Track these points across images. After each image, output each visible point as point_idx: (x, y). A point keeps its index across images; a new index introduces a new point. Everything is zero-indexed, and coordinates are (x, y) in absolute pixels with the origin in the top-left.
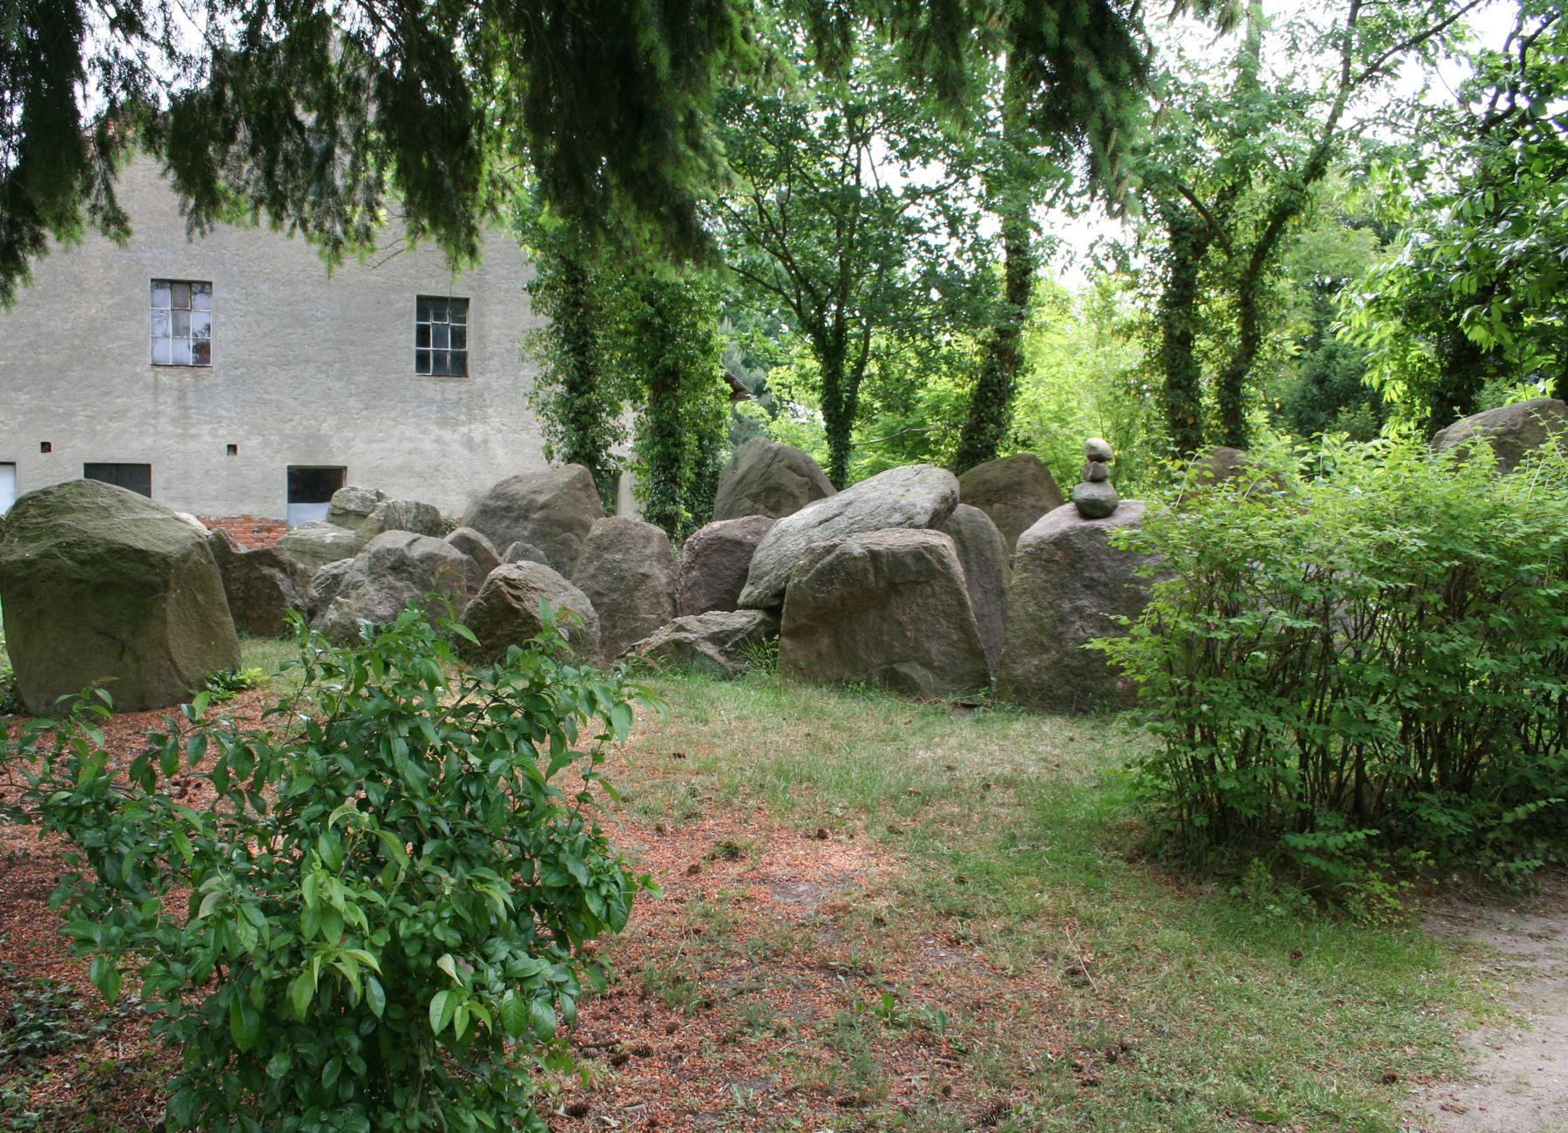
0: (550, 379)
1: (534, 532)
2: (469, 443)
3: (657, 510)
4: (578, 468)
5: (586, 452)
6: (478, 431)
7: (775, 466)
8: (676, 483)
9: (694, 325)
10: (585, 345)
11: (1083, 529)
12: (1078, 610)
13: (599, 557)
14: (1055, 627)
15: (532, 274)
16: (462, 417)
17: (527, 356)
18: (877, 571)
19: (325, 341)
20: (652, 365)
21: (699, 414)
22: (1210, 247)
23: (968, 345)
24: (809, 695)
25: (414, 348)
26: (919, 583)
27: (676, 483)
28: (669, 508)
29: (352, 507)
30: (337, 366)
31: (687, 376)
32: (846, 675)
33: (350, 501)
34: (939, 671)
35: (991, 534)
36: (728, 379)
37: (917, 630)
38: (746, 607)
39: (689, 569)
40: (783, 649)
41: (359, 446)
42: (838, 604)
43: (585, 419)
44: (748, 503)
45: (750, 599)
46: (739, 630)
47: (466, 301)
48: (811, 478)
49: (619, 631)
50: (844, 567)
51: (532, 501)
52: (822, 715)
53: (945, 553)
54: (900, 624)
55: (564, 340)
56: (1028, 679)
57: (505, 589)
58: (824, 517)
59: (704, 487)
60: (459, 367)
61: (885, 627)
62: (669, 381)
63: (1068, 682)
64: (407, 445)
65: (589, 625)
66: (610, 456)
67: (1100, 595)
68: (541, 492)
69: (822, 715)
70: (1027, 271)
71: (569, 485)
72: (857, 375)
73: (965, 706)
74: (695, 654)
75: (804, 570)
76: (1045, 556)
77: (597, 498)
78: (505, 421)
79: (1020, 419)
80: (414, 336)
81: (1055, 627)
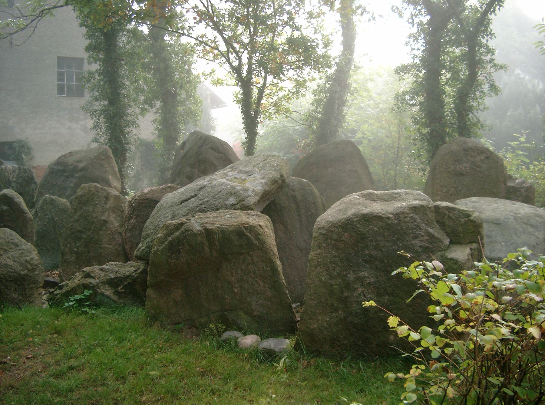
12: (361, 280)
16: (81, 117)
18: (211, 244)
44: (188, 169)
46: (128, 277)
54: (229, 282)
58: (184, 197)
76: (335, 237)
80: (56, 76)
81: (342, 292)
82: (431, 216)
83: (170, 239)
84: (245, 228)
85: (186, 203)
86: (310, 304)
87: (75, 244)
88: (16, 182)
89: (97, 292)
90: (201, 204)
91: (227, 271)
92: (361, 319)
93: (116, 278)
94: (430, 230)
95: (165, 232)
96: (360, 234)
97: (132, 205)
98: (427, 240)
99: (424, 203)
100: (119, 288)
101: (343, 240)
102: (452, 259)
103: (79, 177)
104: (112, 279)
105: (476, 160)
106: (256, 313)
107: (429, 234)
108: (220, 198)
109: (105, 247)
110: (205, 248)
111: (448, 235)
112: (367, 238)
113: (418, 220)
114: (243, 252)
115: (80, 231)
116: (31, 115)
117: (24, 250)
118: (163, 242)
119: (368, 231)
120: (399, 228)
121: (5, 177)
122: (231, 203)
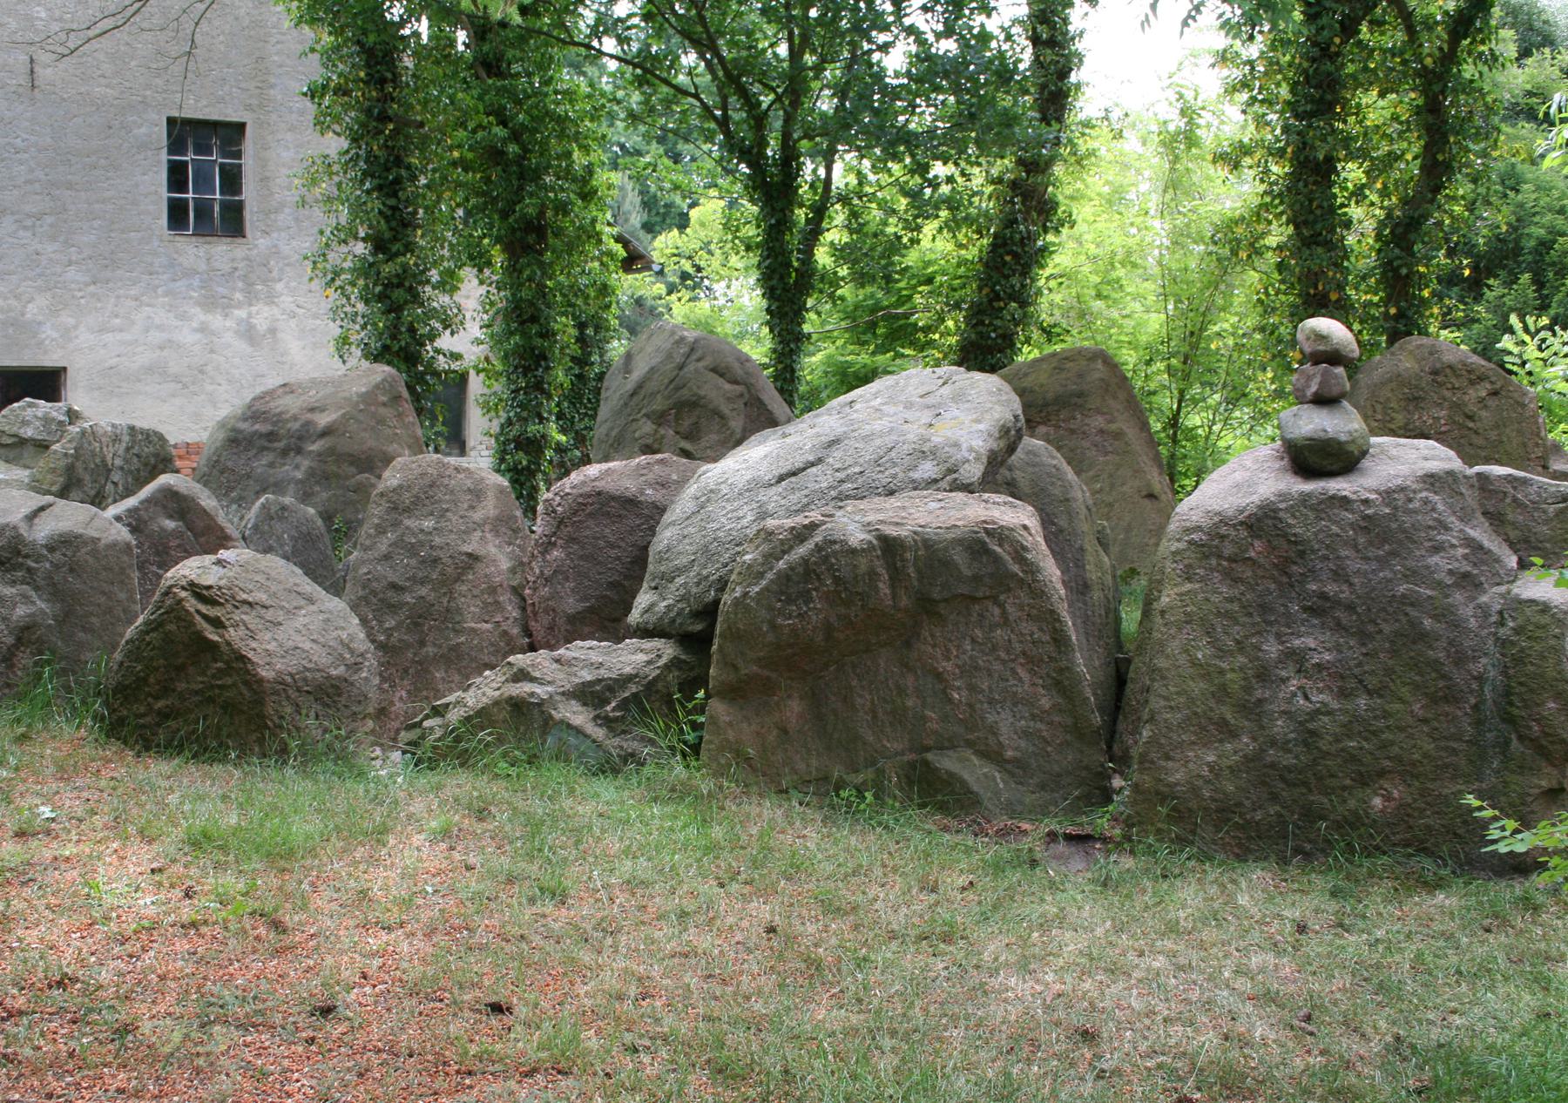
0: (346, 235)
1: (311, 473)
2: (249, 333)
3: (515, 431)
4: (383, 370)
5: (400, 339)
6: (262, 315)
7: (691, 367)
8: (543, 391)
9: (569, 154)
10: (398, 181)
11: (1304, 499)
12: (1296, 658)
13: (396, 524)
14: (1248, 689)
15: (314, 70)
16: (238, 296)
17: (309, 199)
18: (896, 575)
19: (27, 182)
20: (505, 215)
21: (578, 291)
22: (1364, 28)
23: (978, 179)
24: (763, 814)
25: (165, 194)
26: (974, 600)
27: (543, 391)
28: (533, 428)
29: (29, 432)
30: (49, 220)
31: (558, 233)
32: (836, 773)
33: (25, 423)
34: (1016, 768)
35: (1067, 487)
36: (619, 239)
37: (972, 688)
38: (645, 632)
39: (547, 546)
40: (713, 720)
41: (84, 337)
42: (819, 638)
43: (399, 294)
44: (647, 427)
45: (652, 619)
46: (630, 678)
47: (240, 128)
48: (749, 386)
49: (430, 650)
50: (831, 568)
51: (308, 423)
52: (796, 869)
53: (1028, 541)
54: (939, 676)
55: (365, 174)
56: (1195, 790)
57: (192, 604)
59: (588, 395)
60: (233, 223)
61: (910, 681)
62: (531, 239)
63: (1274, 798)
64: (156, 337)
65: (356, 667)
66: (438, 351)
67: (1339, 626)
68: (322, 410)
69: (796, 869)
70: (1064, 74)
71: (368, 398)
72: (814, 232)
73: (1070, 838)
74: (548, 724)
75: (752, 573)
76: (1228, 550)
77: (412, 417)
78: (301, 300)
79: (1051, 298)
80: (163, 176)
81: (1248, 689)
82: (1471, 497)
83: (781, 564)
84: (987, 531)
85: (793, 479)
86: (1166, 721)
87: (381, 622)
88: (122, 468)
89: (551, 717)
90: (842, 481)
91: (934, 646)
92: (1296, 757)
93: (599, 681)
94: (1472, 533)
95: (765, 548)
96: (1295, 543)
97: (554, 511)
98: (1465, 557)
99: (1447, 466)
100: (608, 708)
101: (1250, 559)
102: (1532, 602)
103: (320, 455)
104: (586, 684)
105: (1467, 398)
106: (1010, 753)
107: (1469, 542)
108: (895, 465)
109: (473, 630)
110: (881, 585)
111: (1512, 546)
112: (1313, 551)
113: (1440, 507)
114: (980, 594)
115: (394, 586)
116: (92, 288)
117: (330, 612)
118: (761, 575)
119: (1316, 534)
120: (1394, 526)
121: (94, 455)
122: (926, 476)
